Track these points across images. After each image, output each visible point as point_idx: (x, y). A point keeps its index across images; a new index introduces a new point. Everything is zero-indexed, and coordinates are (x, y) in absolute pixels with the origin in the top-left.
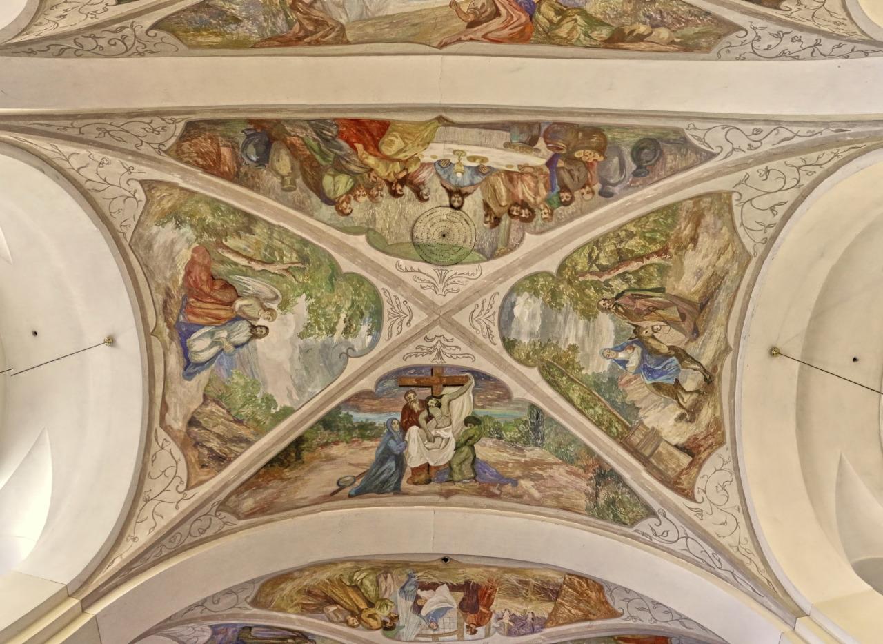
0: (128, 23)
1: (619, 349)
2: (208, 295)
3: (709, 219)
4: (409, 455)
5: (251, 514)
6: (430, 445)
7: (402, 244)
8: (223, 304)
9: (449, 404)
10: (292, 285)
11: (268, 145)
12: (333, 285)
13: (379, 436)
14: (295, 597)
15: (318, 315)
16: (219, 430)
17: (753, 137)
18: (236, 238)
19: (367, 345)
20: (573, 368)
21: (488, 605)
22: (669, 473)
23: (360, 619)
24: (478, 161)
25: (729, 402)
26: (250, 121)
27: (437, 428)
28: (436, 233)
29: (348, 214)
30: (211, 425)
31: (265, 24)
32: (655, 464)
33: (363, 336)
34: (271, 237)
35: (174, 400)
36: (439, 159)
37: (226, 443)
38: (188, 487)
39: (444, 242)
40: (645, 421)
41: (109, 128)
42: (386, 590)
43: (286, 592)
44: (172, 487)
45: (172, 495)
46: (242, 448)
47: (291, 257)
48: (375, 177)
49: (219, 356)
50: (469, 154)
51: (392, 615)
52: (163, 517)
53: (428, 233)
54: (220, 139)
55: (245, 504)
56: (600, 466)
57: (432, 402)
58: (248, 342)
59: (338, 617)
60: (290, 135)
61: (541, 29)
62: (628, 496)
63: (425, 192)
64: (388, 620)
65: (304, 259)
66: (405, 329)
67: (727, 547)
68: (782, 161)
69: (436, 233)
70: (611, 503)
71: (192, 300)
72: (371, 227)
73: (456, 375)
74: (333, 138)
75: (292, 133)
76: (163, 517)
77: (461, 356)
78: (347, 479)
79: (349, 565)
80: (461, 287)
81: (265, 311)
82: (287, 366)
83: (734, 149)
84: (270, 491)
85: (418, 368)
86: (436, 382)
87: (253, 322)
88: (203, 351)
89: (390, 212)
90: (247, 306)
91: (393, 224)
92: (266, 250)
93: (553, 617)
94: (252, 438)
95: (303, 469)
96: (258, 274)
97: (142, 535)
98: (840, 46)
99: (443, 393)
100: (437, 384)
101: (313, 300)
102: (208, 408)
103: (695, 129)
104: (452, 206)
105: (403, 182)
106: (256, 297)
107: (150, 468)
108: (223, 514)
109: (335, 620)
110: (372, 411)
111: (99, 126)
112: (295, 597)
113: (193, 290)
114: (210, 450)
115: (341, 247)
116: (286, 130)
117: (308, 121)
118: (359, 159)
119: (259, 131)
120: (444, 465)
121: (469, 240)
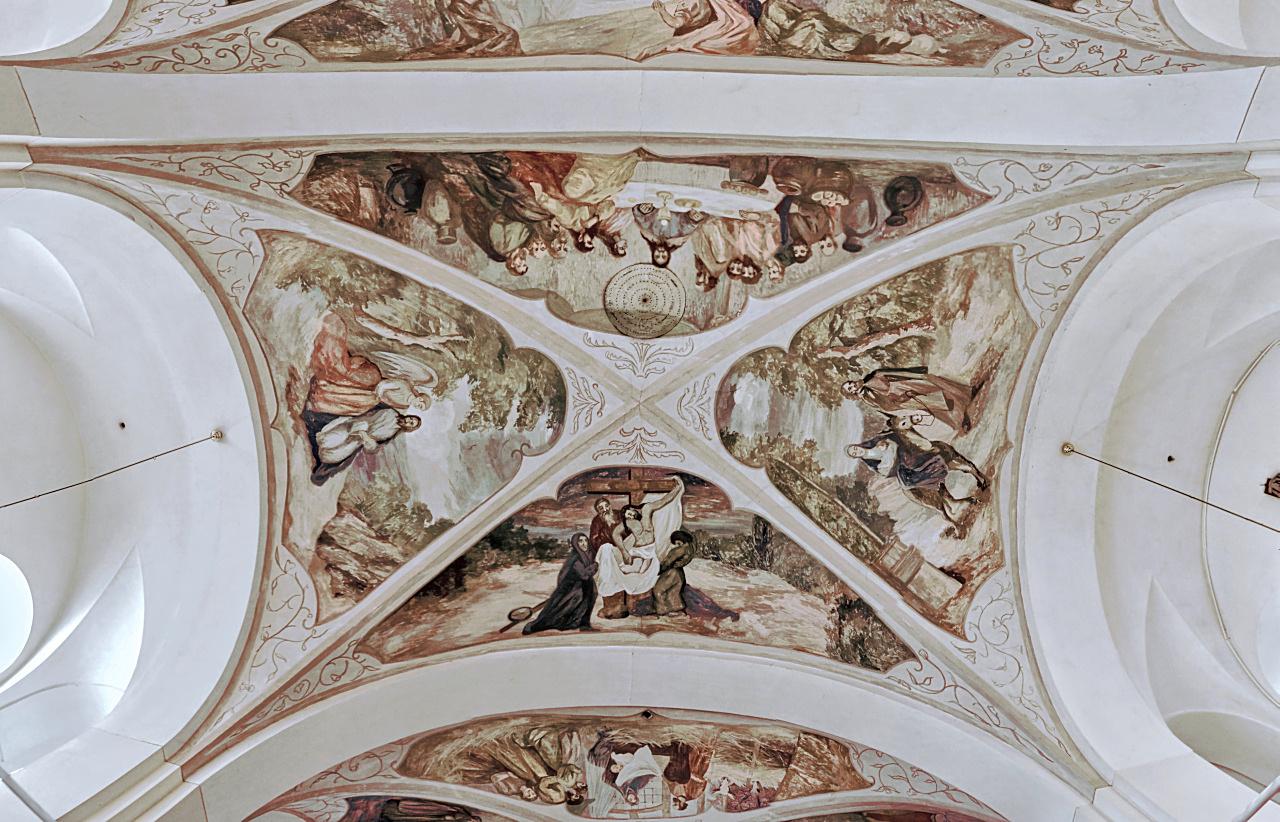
1: (869, 445)
2: (343, 377)
3: (983, 279)
5: (398, 656)
6: (627, 568)
9: (651, 516)
10: (451, 363)
15: (484, 403)
17: (1040, 175)
19: (547, 440)
20: (810, 470)
21: (701, 773)
22: (933, 603)
23: (537, 791)
25: (1010, 514)
30: (347, 542)
32: (915, 592)
34: (424, 303)
38: (317, 622)
40: (902, 537)
42: (571, 752)
43: (444, 756)
45: (297, 632)
46: (387, 571)
47: (449, 329)
49: (358, 455)
50: (677, 197)
51: (579, 785)
53: (625, 299)
56: (845, 595)
57: (629, 513)
58: (394, 436)
59: (509, 788)
61: (769, 37)
62: (880, 633)
63: (620, 244)
64: (574, 792)
65: (466, 330)
66: (596, 418)
67: (1008, 698)
68: (1077, 206)
70: (858, 641)
72: (551, 289)
78: (521, 611)
79: (523, 721)
81: (416, 396)
82: (445, 466)
83: (1015, 190)
84: (423, 626)
86: (635, 487)
87: (401, 412)
93: (784, 788)
94: (399, 558)
95: (465, 598)
96: (408, 349)
97: (258, 685)
98: (1151, 58)
101: (478, 383)
103: (966, 164)
104: (655, 263)
105: (593, 232)
106: (405, 378)
107: (268, 596)
108: (363, 656)
109: (506, 791)
114: (347, 574)
118: (537, 203)
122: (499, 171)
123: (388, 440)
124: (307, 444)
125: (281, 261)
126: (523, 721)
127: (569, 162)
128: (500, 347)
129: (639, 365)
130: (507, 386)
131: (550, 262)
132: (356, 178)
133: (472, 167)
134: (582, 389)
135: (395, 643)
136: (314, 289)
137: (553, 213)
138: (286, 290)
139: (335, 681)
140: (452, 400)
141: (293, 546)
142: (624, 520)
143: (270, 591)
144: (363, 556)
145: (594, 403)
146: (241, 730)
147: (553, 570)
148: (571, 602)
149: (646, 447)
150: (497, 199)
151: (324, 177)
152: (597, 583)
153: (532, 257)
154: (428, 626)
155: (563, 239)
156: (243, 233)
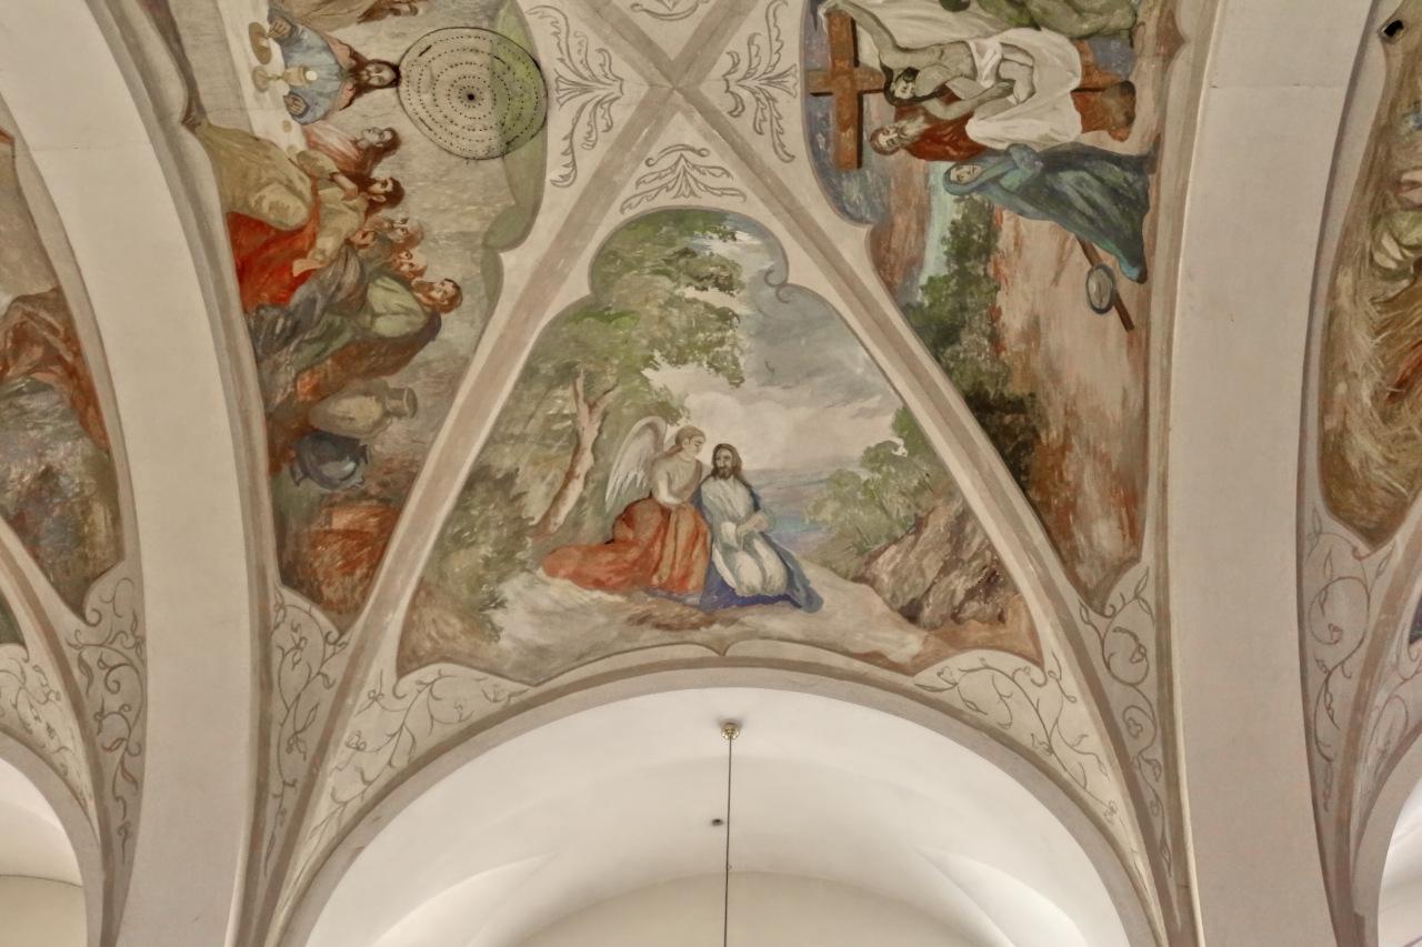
0: (71, 654)
2: (647, 553)
4: (1047, 138)
5: (1133, 531)
6: (1021, 90)
7: (509, 178)
8: (665, 525)
9: (906, 50)
10: (624, 396)
11: (319, 436)
12: (621, 315)
13: (991, 210)
14: (1399, 430)
15: (692, 345)
16: (932, 567)
18: (524, 500)
19: (757, 242)
24: (264, 43)
26: (274, 469)
27: (974, 74)
28: (469, 114)
29: (456, 287)
30: (919, 580)
31: (49, 429)
33: (738, 249)
34: (522, 438)
35: (860, 637)
36: (289, 118)
37: (959, 560)
38: (1038, 661)
39: (487, 95)
41: (288, 730)
44: (1034, 693)
45: (1048, 697)
46: (974, 531)
47: (564, 400)
48: (364, 236)
49: (776, 541)
50: (256, 63)
52: (1086, 736)
53: (476, 128)
54: (314, 528)
55: (1105, 543)
57: (901, 90)
58: (747, 486)
60: (291, 397)
63: (374, 138)
65: (566, 374)
66: (714, 159)
69: (469, 114)
71: (655, 580)
72: (479, 241)
73: (825, 40)
74: (288, 315)
75: (289, 390)
76: (1086, 736)
77: (774, 34)
78: (1093, 287)
79: (1346, 281)
80: (593, 47)
81: (680, 449)
82: (802, 413)
85: (812, 127)
86: (848, 85)
87: (706, 473)
88: (763, 570)
89: (440, 204)
90: (670, 482)
91: (466, 196)
92: (550, 447)
94: (956, 506)
95: (1048, 396)
96: (601, 460)
99: (877, 66)
100: (853, 82)
101: (657, 354)
102: (885, 578)
104: (395, 82)
105: (363, 181)
106: (650, 465)
108: (1114, 598)
110: (922, 231)
111: (284, 746)
112: (1399, 430)
113: (638, 576)
114: (971, 594)
115: (531, 302)
116: (282, 404)
117: (258, 361)
118: (329, 266)
119: (293, 454)
120: (1081, 53)
121: (472, 42)
122: (281, 321)
123: (753, 495)
124: (754, 609)
125: (454, 639)
126: (1346, 281)
127: (241, 224)
128: (592, 320)
129: (600, 93)
130: (660, 306)
131: (432, 244)
132: (317, 533)
133: (282, 359)
134: (658, 183)
135: (1104, 534)
136: (502, 592)
137: (342, 240)
138: (502, 629)
139: (1144, 655)
140: (687, 395)
141: (918, 661)
142: (915, 100)
143: (980, 715)
144: (945, 562)
145: (683, 160)
146: (1165, 851)
147: (1016, 228)
148: (1088, 192)
149: (761, 69)
150: (330, 325)
151: (317, 580)
152: (1051, 144)
153: (427, 273)
154: (1088, 471)
155: (386, 225)
156: (400, 694)
